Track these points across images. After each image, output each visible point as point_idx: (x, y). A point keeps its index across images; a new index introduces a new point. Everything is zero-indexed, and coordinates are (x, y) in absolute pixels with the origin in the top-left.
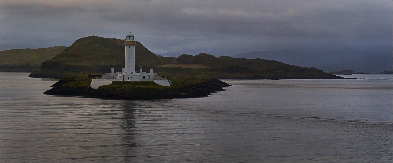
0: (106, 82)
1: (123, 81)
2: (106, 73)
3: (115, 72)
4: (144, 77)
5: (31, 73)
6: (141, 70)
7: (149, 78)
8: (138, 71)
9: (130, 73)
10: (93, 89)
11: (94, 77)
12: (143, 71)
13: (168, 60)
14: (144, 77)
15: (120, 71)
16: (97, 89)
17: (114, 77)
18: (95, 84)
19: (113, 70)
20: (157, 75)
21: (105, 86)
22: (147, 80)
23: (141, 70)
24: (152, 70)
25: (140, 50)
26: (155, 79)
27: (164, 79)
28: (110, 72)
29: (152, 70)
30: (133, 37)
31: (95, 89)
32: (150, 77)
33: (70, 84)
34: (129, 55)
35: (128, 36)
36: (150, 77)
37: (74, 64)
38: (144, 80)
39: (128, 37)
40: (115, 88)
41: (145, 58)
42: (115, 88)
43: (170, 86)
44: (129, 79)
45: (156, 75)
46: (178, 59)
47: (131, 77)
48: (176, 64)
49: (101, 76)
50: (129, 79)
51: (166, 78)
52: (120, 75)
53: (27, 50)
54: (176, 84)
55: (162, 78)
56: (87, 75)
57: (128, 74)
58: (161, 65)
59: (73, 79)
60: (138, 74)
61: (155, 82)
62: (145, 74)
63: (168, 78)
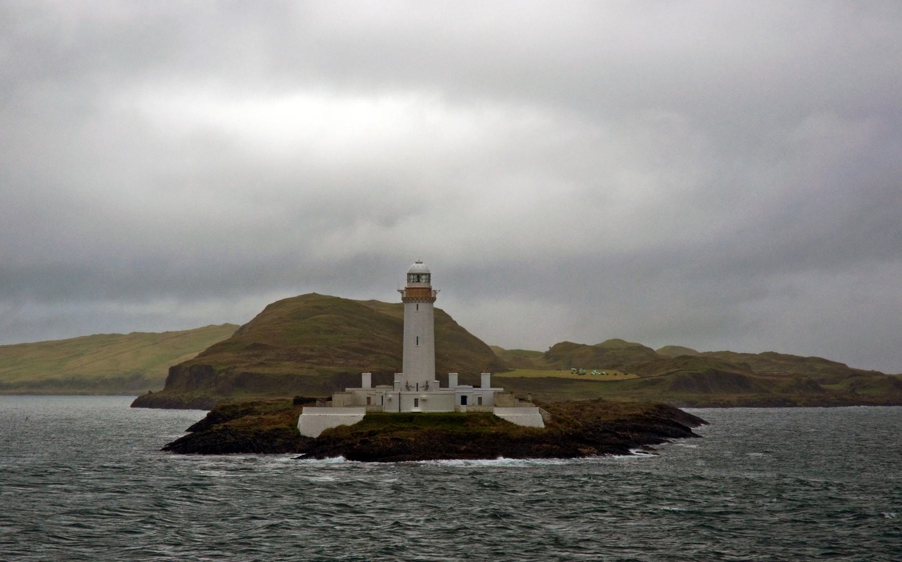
0: (344, 415)
1: (397, 411)
2: (347, 389)
3: (373, 386)
4: (464, 400)
5: (200, 415)
6: (453, 378)
7: (477, 404)
8: (444, 382)
9: (419, 390)
10: (305, 437)
11: (301, 402)
12: (461, 382)
13: (521, 357)
14: (464, 400)
15: (390, 381)
16: (318, 438)
17: (369, 399)
18: (312, 422)
19: (367, 379)
20: (503, 393)
21: (341, 428)
22: (471, 409)
23: (453, 378)
24: (486, 378)
25: (447, 331)
26: (496, 406)
27: (526, 406)
28: (358, 384)
29: (486, 378)
30: (429, 275)
31: (311, 438)
32: (480, 399)
33: (234, 423)
34: (418, 359)
35: (414, 274)
36: (480, 399)
37: (259, 370)
38: (463, 409)
39: (412, 277)
40: (372, 434)
41: (458, 351)
42: (375, 435)
43: (542, 426)
44: (416, 405)
45: (499, 393)
46: (547, 355)
47: (424, 400)
48: (541, 368)
49: (330, 399)
50: (416, 405)
51: (529, 402)
52: (391, 394)
53: (135, 337)
54: (560, 421)
55: (517, 401)
56: (291, 399)
57: (413, 391)
58: (507, 370)
59: (249, 409)
60: (444, 391)
61: (500, 413)
62: (467, 390)
63: (536, 403)
